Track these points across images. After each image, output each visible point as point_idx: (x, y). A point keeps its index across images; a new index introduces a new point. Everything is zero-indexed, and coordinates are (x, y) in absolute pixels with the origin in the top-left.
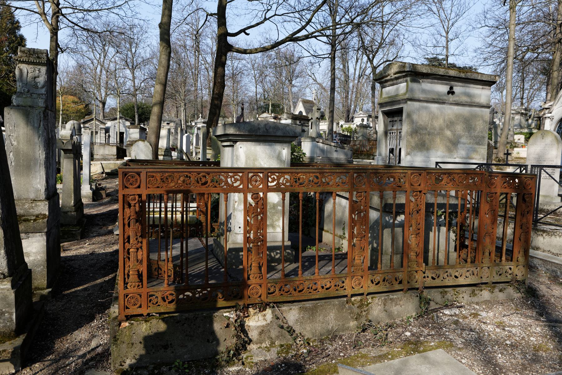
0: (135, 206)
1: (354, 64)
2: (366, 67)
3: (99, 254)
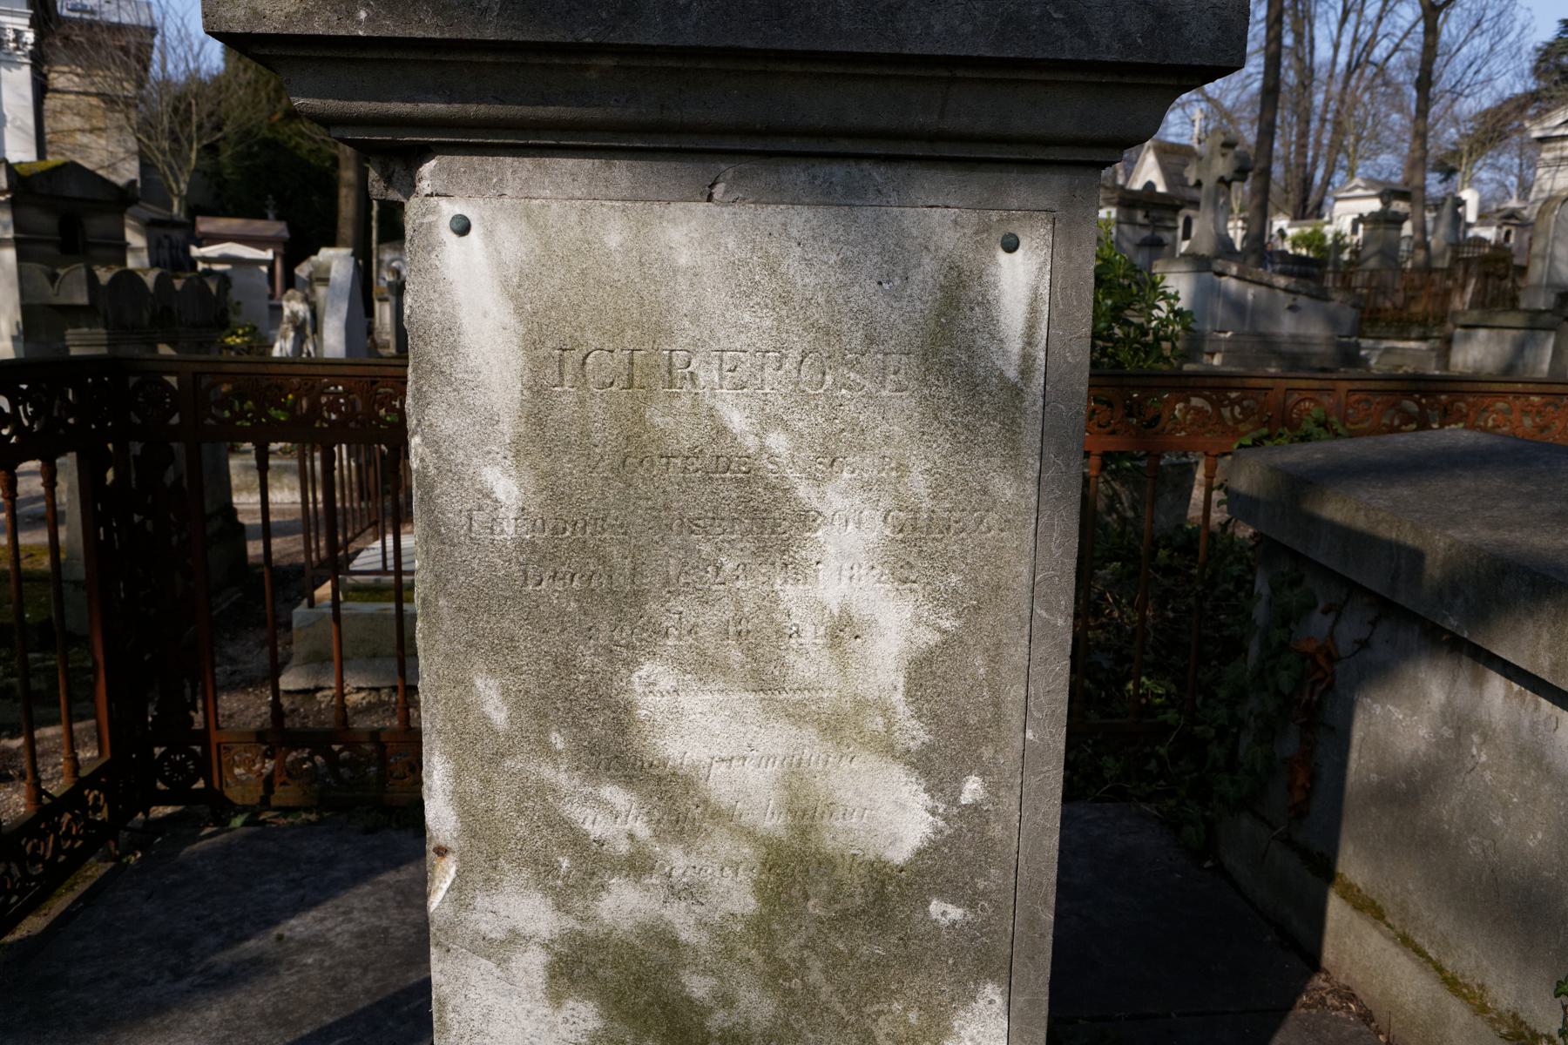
1: (1334, 28)
2: (1374, 36)
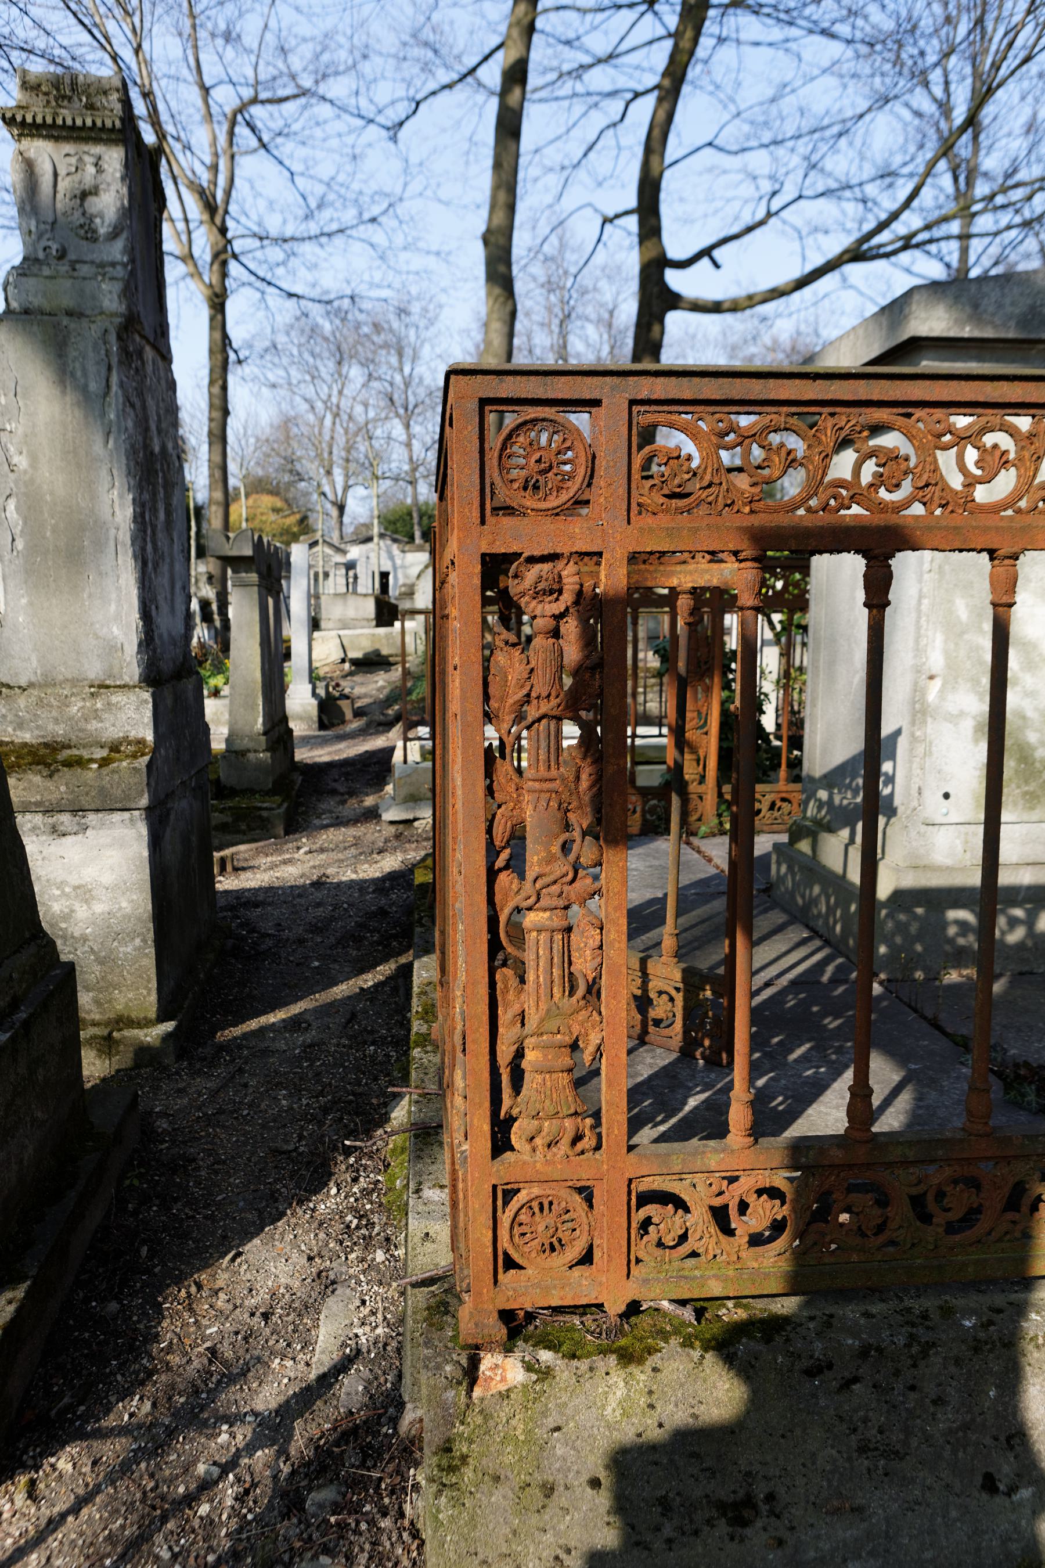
0: (556, 634)
3: (339, 884)
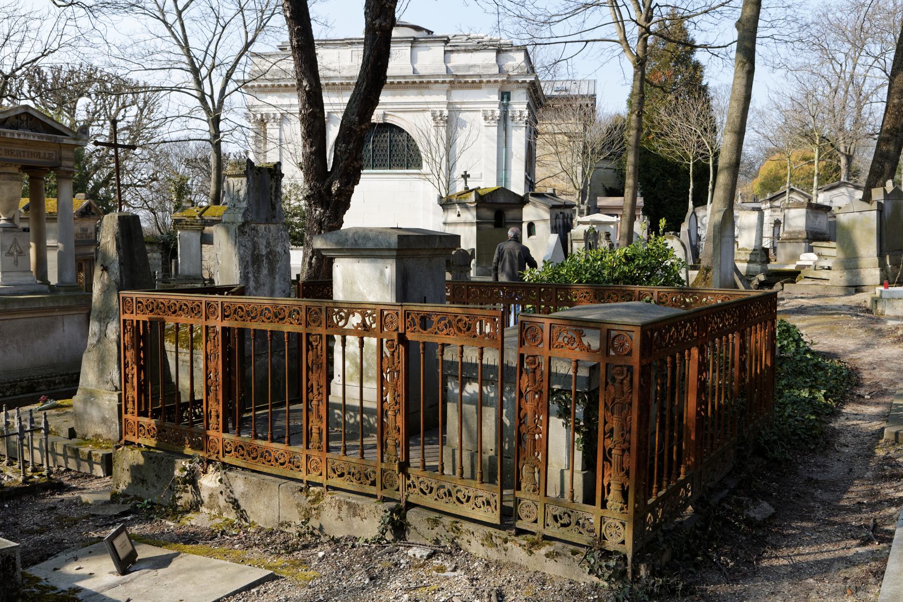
0: (622, 383)
